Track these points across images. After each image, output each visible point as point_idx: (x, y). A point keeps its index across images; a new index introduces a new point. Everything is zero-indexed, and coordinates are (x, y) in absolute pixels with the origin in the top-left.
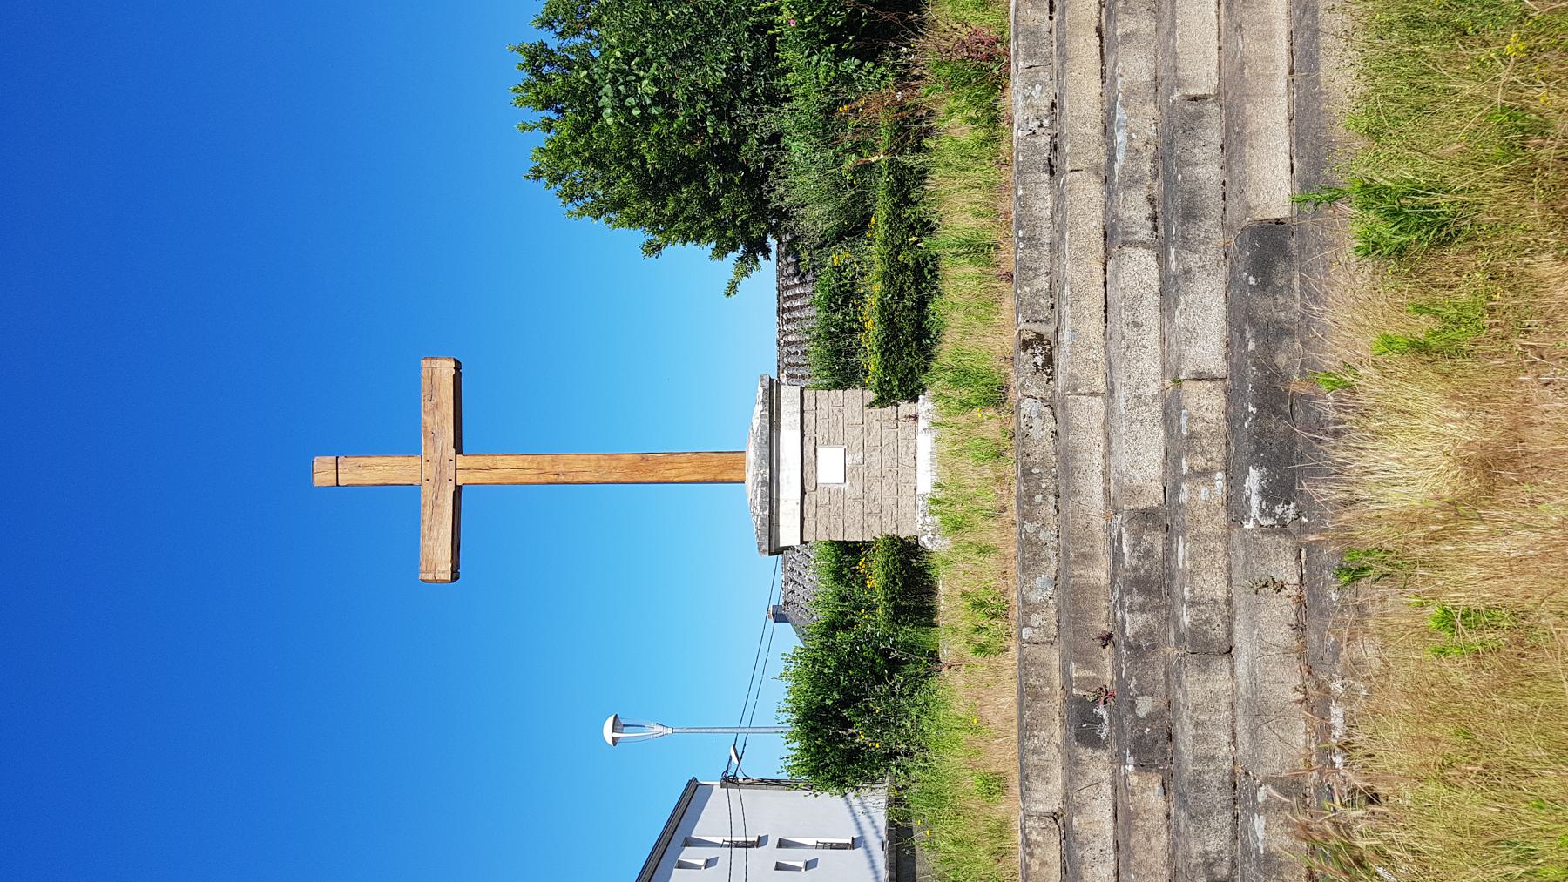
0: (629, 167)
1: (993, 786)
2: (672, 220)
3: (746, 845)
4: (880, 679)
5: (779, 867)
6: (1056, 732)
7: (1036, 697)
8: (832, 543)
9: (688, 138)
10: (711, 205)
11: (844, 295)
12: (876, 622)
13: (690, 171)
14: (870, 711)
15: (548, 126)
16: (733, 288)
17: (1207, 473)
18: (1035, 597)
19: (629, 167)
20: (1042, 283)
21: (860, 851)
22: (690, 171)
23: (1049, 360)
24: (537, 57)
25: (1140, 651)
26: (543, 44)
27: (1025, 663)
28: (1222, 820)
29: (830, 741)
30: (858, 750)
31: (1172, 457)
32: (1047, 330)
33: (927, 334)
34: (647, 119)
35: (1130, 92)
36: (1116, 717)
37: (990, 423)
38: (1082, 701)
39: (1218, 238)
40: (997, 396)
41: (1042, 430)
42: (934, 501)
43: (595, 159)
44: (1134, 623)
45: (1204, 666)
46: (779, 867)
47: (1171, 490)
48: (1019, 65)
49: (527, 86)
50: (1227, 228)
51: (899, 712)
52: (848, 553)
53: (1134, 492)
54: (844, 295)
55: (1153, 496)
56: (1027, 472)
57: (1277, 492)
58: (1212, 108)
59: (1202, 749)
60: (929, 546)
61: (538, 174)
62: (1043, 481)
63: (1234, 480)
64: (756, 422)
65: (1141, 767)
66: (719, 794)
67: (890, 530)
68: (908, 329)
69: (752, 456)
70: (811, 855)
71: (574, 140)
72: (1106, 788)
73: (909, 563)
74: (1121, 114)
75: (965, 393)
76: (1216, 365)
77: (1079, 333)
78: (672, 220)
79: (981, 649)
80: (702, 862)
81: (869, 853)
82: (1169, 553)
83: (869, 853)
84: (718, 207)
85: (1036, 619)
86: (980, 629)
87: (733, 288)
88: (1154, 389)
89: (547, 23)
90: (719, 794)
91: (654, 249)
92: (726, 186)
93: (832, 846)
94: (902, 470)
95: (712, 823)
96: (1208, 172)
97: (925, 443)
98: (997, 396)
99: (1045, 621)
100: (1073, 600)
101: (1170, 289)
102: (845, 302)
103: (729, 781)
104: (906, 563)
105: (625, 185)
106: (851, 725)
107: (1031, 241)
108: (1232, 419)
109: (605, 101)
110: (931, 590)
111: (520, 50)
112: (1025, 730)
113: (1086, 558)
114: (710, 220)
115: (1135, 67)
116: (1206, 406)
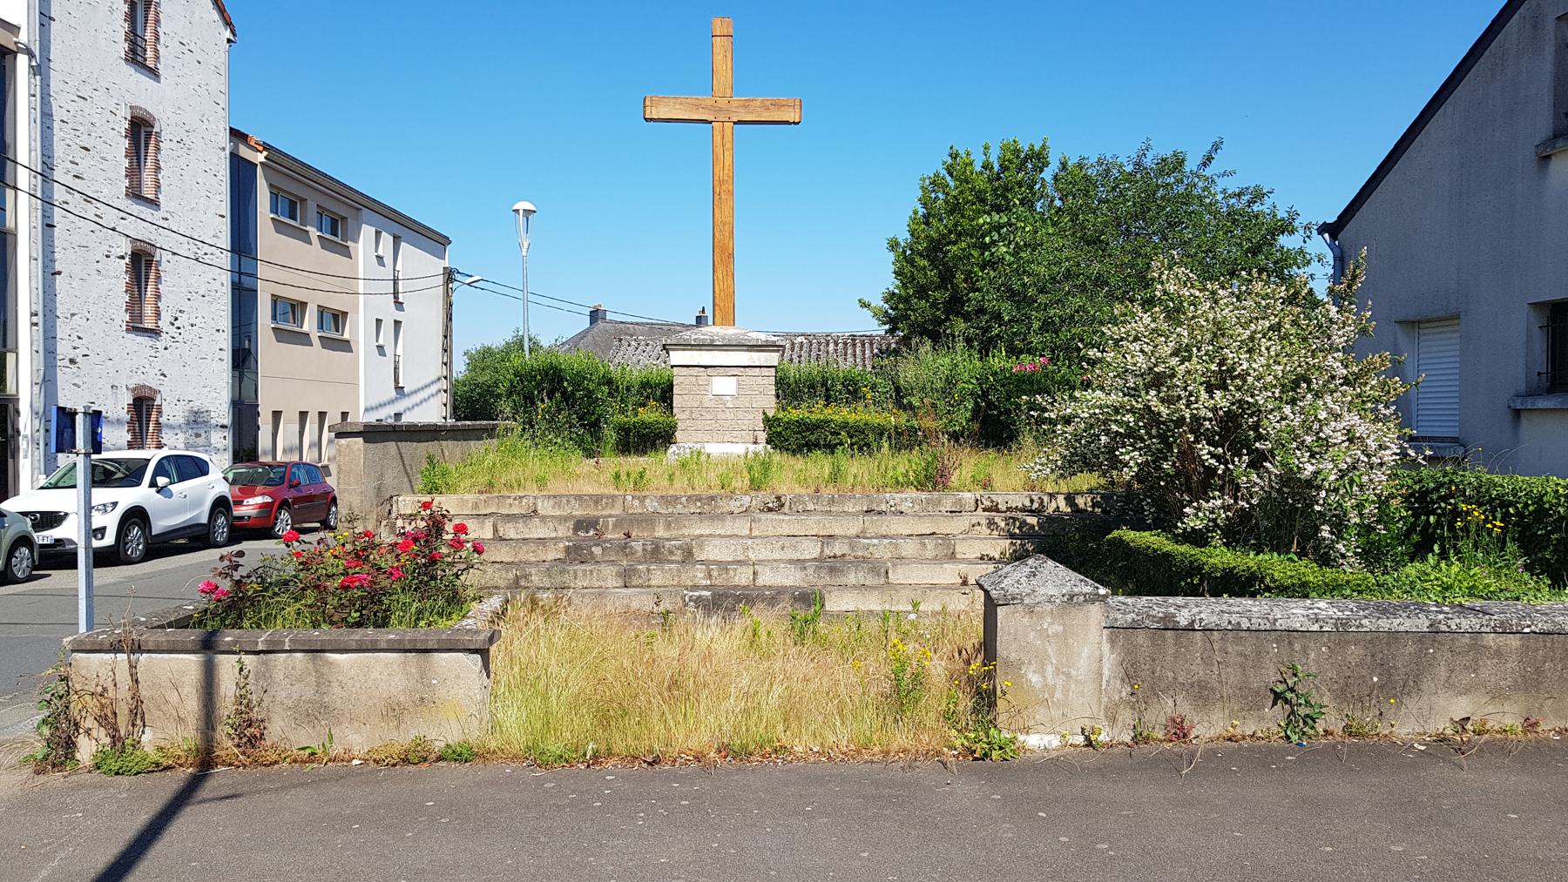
0: (950, 232)
1: (541, 482)
2: (911, 262)
3: (396, 294)
4: (581, 418)
5: (379, 322)
6: (579, 512)
7: (596, 502)
8: (671, 386)
9: (969, 277)
10: (922, 292)
11: (853, 391)
12: (615, 417)
13: (946, 278)
14: (559, 411)
15: (987, 166)
16: (865, 305)
17: (710, 576)
18: (648, 501)
19: (950, 232)
20: (810, 507)
21: (393, 394)
22: (946, 278)
23: (770, 510)
24: (1038, 158)
25: (624, 548)
26: (1047, 164)
27: (613, 497)
28: (547, 583)
29: (539, 384)
30: (533, 403)
31: (718, 563)
32: (786, 509)
33: (809, 450)
34: (984, 247)
35: (896, 546)
36: (590, 539)
37: (742, 482)
38: (597, 523)
39: (820, 583)
40: (755, 486)
41: (734, 506)
42: (699, 453)
43: (955, 208)
44: (637, 546)
45: (619, 575)
46: (379, 322)
47: (702, 562)
48: (924, 495)
49: (1017, 152)
50: (824, 586)
51: (558, 431)
52: (665, 394)
53: (701, 546)
54: (853, 391)
55: (699, 555)
56: (713, 498)
57: (698, 601)
58: (882, 580)
59: (580, 574)
60: (670, 451)
61: (954, 156)
62: (708, 506)
63: (706, 588)
64: (754, 335)
65: (568, 548)
66: (436, 266)
67: (680, 425)
68: (813, 438)
69: (730, 332)
70: (389, 350)
71: (972, 190)
72: (553, 535)
73: (654, 439)
74: (886, 541)
75: (757, 468)
76: (760, 582)
77: (783, 524)
78: (911, 262)
79: (617, 476)
80: (380, 253)
81: (392, 402)
82: (671, 562)
83: (392, 402)
84: (920, 298)
85: (636, 502)
86: (628, 475)
87: (865, 305)
88: (752, 556)
89: (1064, 166)
90: (436, 266)
91: (894, 245)
92: (934, 305)
93: (396, 369)
94: (721, 434)
95: (416, 262)
96: (852, 578)
97: (739, 449)
98: (755, 486)
99: (635, 507)
100: (648, 520)
101: (800, 563)
102: (849, 392)
103: (449, 275)
104: (658, 436)
105: (937, 228)
106: (550, 398)
107: (832, 501)
108: (736, 587)
109: (996, 217)
110: (644, 453)
111: (1044, 147)
112: (579, 497)
113: (668, 526)
114: (911, 292)
115: (909, 548)
116: (742, 577)
